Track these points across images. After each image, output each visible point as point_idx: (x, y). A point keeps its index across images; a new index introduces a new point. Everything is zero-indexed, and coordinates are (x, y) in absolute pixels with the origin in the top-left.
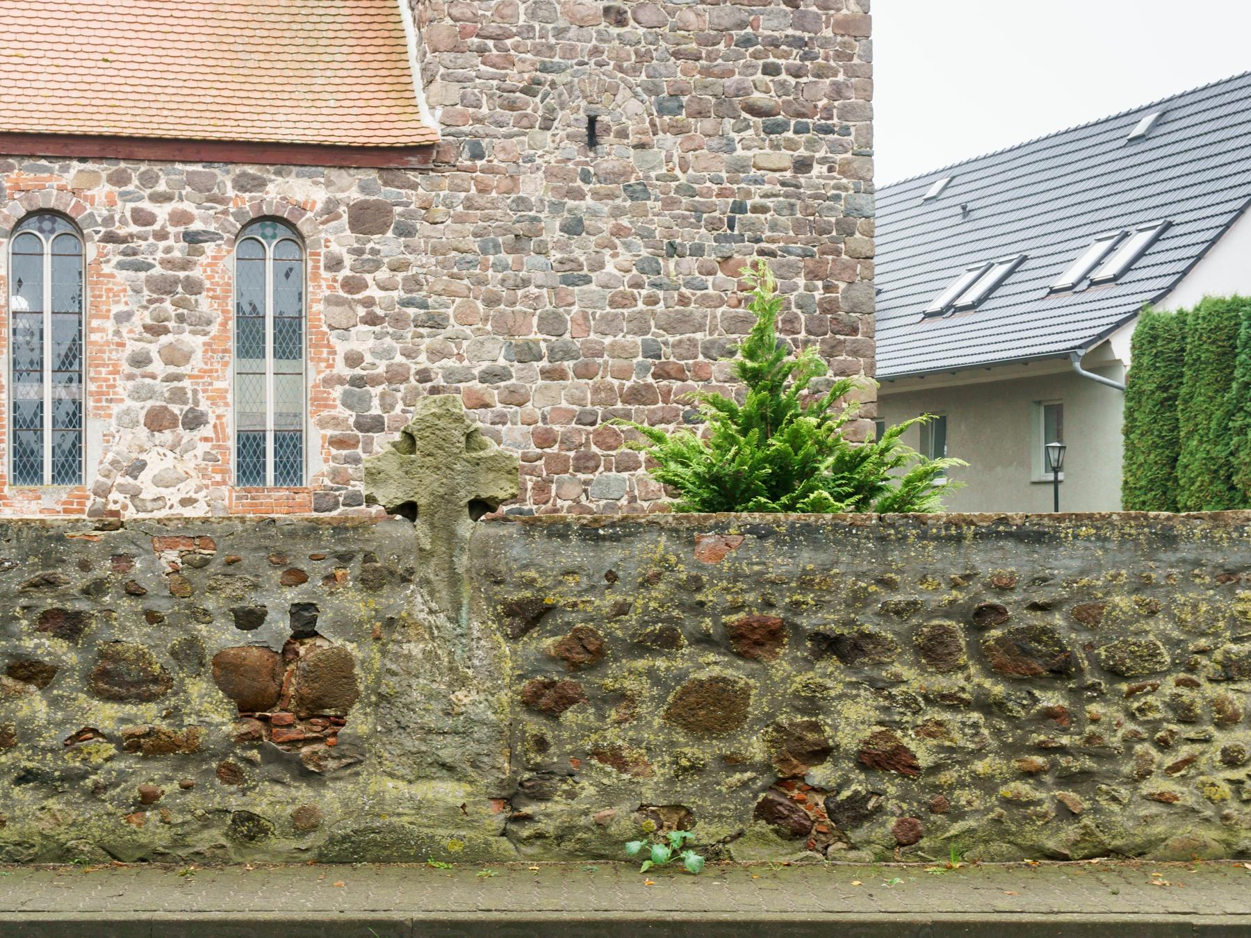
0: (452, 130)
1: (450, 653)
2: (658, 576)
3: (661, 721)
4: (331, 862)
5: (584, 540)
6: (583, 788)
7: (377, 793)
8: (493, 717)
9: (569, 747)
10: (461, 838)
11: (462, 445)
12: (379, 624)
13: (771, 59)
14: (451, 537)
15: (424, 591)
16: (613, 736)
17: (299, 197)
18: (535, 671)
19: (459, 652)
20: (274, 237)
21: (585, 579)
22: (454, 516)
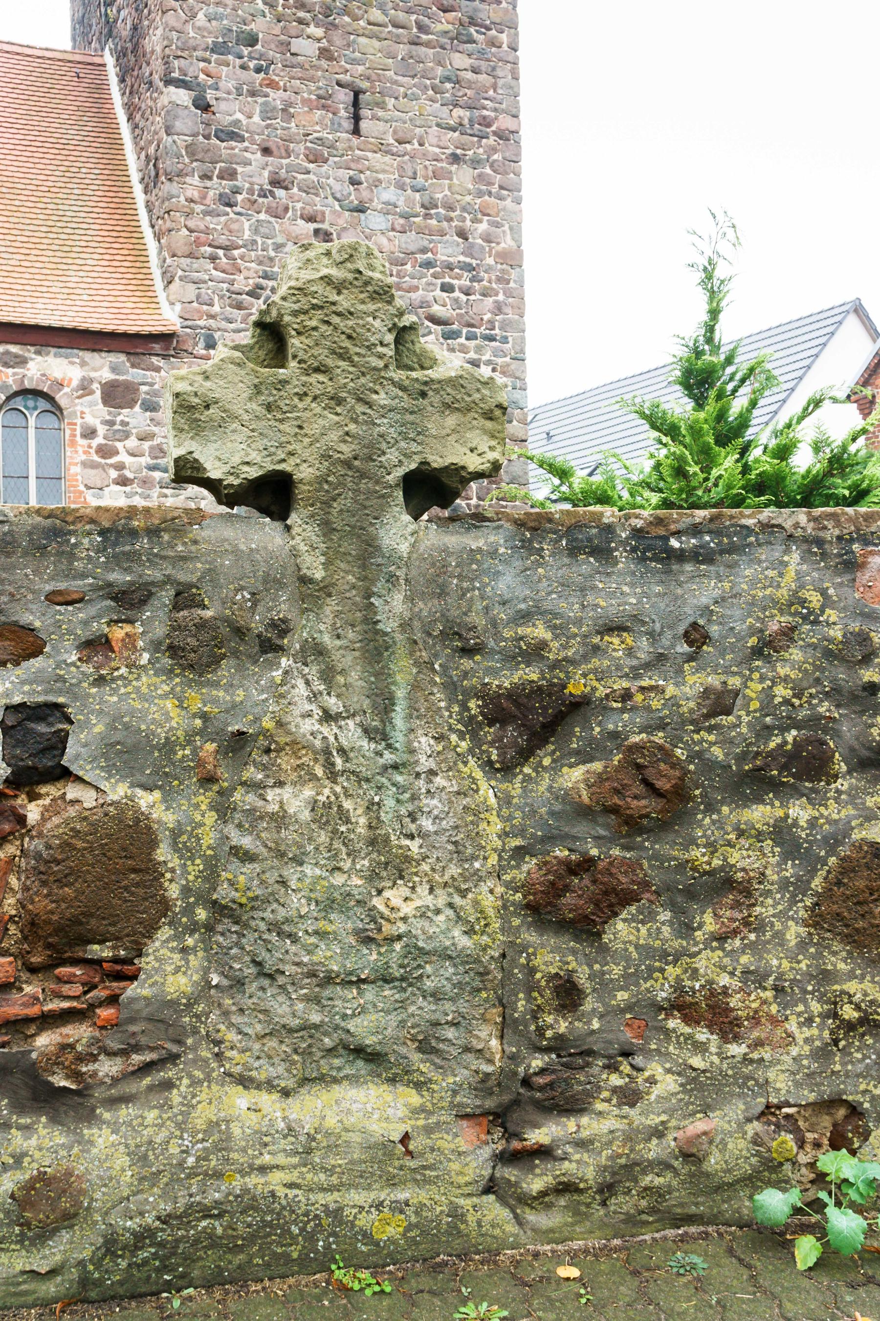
0: (189, 323)
1: (372, 807)
2: (789, 633)
3: (803, 930)
4: (109, 1299)
5: (643, 559)
6: (652, 1081)
7: (213, 1125)
8: (464, 942)
9: (622, 996)
10: (399, 1207)
11: (390, 352)
12: (211, 747)
13: (447, 280)
14: (368, 551)
15: (312, 671)
16: (712, 968)
17: (58, 374)
18: (550, 839)
19: (390, 803)
20: (35, 408)
21: (644, 642)
22: (370, 509)
